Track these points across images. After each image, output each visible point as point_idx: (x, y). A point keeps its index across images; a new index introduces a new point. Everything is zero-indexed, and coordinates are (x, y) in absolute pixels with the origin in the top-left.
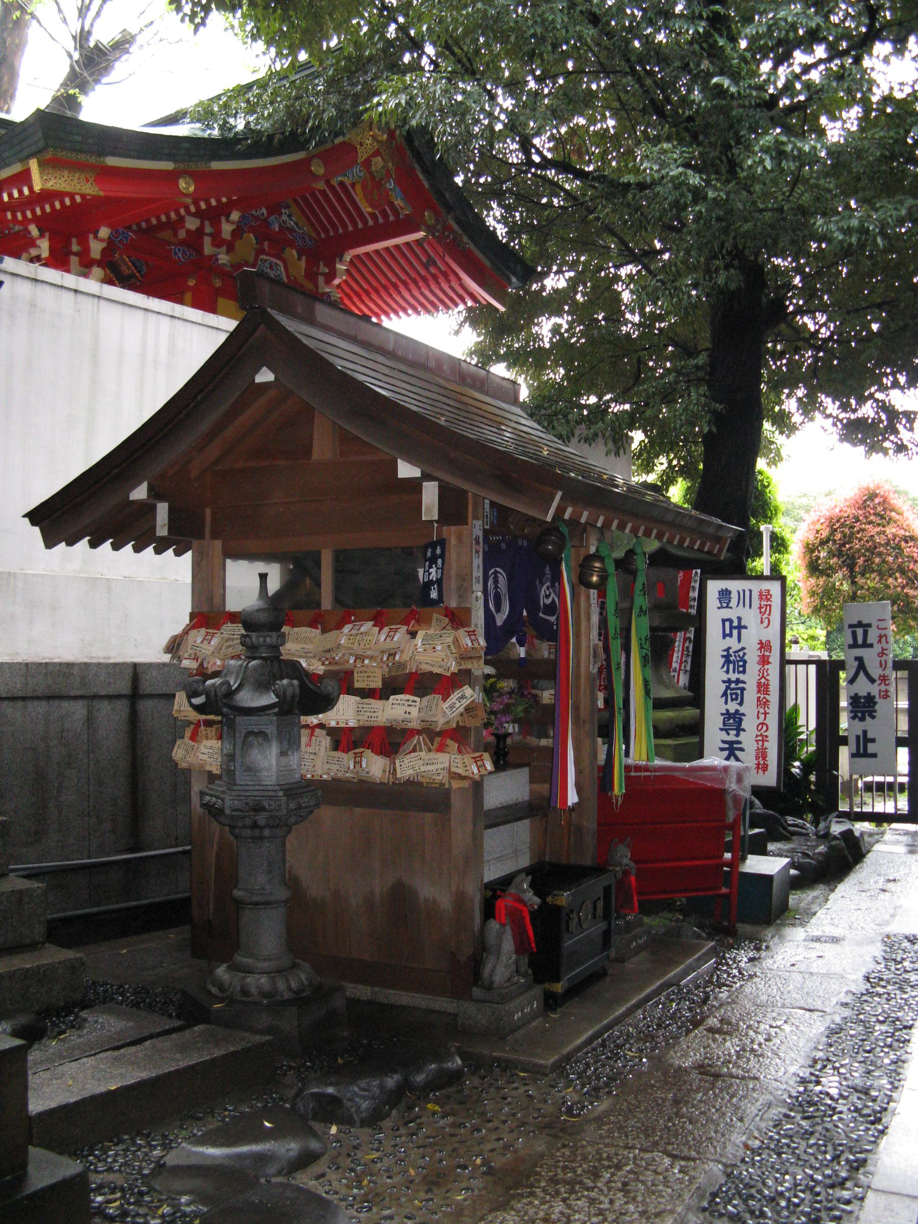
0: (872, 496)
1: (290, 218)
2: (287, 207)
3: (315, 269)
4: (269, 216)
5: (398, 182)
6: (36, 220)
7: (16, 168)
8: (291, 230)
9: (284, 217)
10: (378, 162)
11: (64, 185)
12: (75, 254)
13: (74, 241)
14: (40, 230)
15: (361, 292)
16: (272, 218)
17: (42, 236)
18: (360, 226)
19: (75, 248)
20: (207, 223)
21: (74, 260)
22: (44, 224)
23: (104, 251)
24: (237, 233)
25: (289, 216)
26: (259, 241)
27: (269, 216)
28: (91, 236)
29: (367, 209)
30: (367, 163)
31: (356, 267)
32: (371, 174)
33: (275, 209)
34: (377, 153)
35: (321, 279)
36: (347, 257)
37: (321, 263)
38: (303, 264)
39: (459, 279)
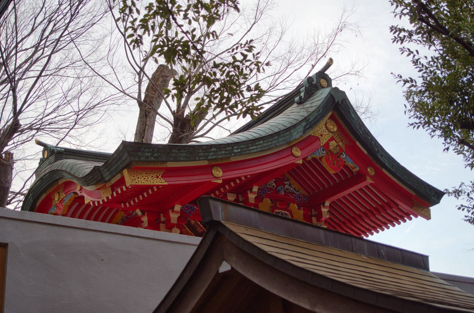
0: (420, 107)
1: (291, 186)
2: (288, 180)
3: (309, 214)
4: (277, 187)
5: (347, 154)
6: (140, 205)
7: (118, 177)
8: (292, 193)
9: (287, 186)
10: (333, 144)
11: (144, 181)
12: (163, 223)
13: (162, 215)
14: (142, 211)
15: (341, 224)
16: (279, 188)
17: (143, 214)
18: (332, 184)
19: (163, 219)
20: (240, 196)
21: (162, 226)
22: (143, 206)
23: (179, 219)
24: (259, 199)
25: (290, 185)
26: (274, 201)
27: (277, 187)
28: (170, 211)
29: (332, 172)
30: (327, 146)
31: (333, 208)
32: (330, 151)
33: (280, 182)
34: (332, 139)
35: (314, 219)
36: (327, 203)
37: (313, 210)
38: (302, 212)
39: (397, 205)
